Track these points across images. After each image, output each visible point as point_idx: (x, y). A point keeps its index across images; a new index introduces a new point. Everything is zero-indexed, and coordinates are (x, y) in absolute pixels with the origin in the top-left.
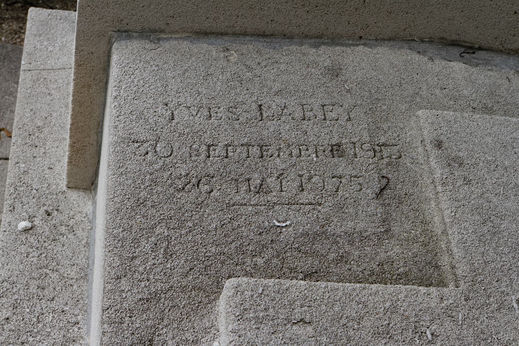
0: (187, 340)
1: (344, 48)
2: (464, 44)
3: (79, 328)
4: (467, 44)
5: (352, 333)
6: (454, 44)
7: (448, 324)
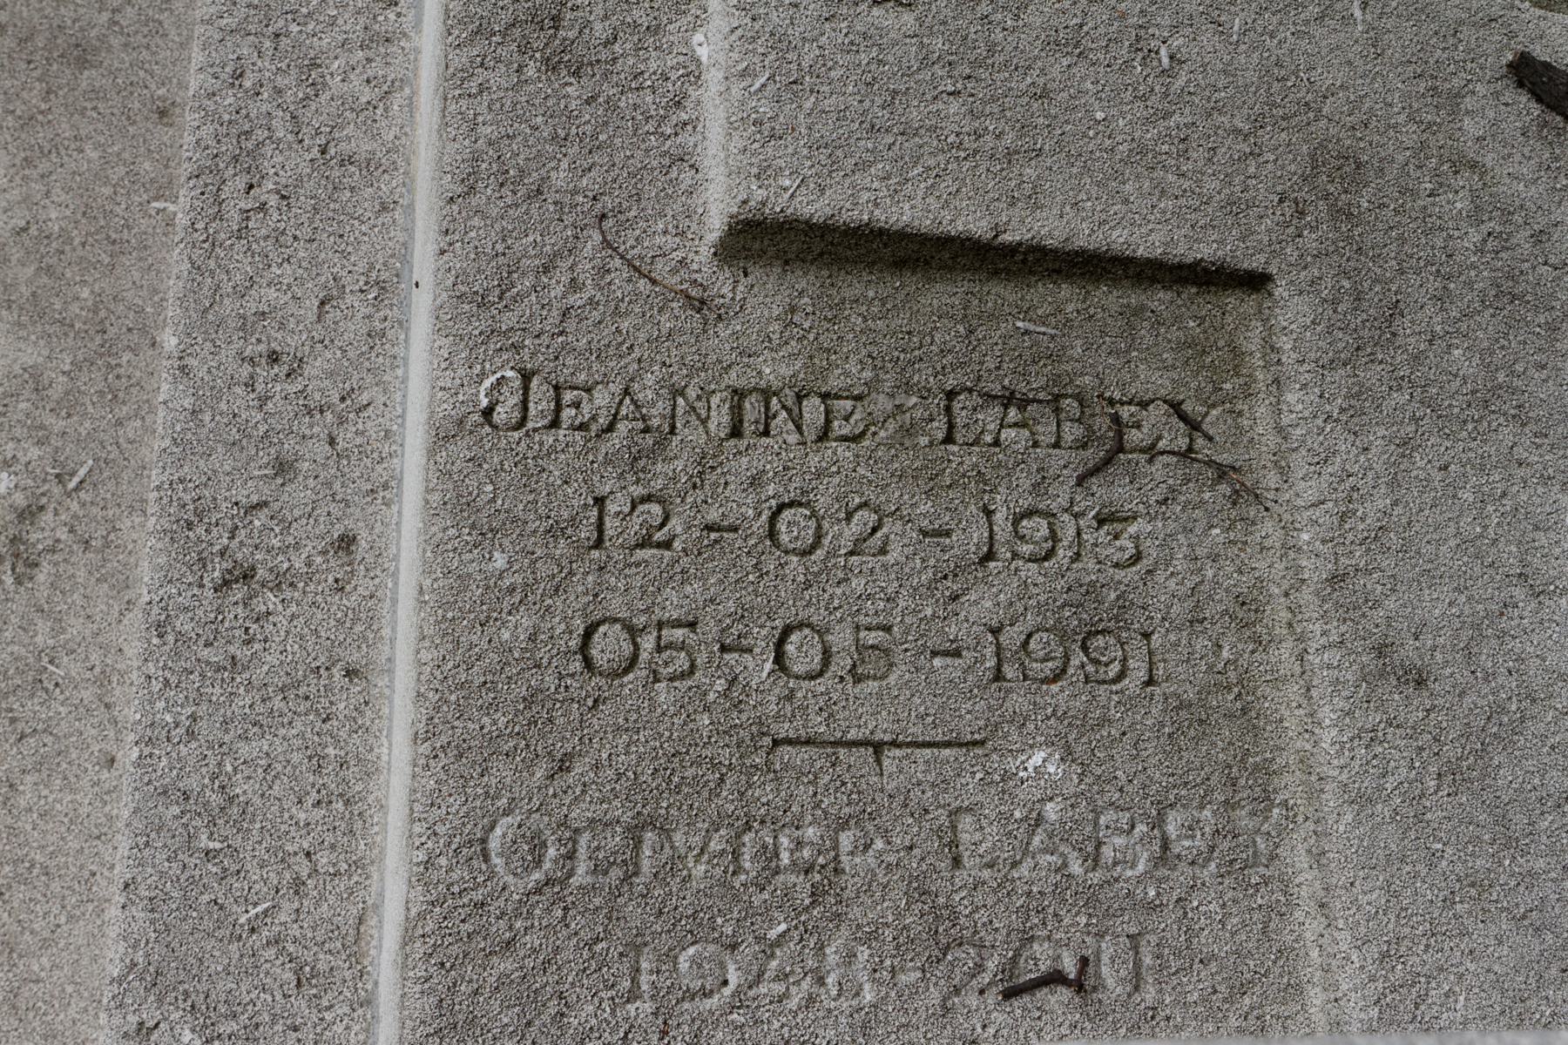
0: (636, 25)
3: (399, 15)
5: (999, 36)
7: (1208, 39)
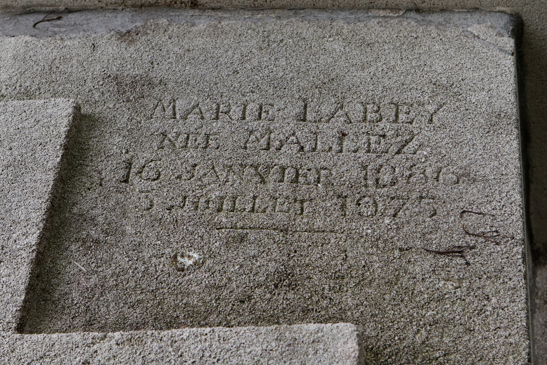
1: (523, 293)
2: (43, 9)
4: (48, 8)
6: (28, 11)
